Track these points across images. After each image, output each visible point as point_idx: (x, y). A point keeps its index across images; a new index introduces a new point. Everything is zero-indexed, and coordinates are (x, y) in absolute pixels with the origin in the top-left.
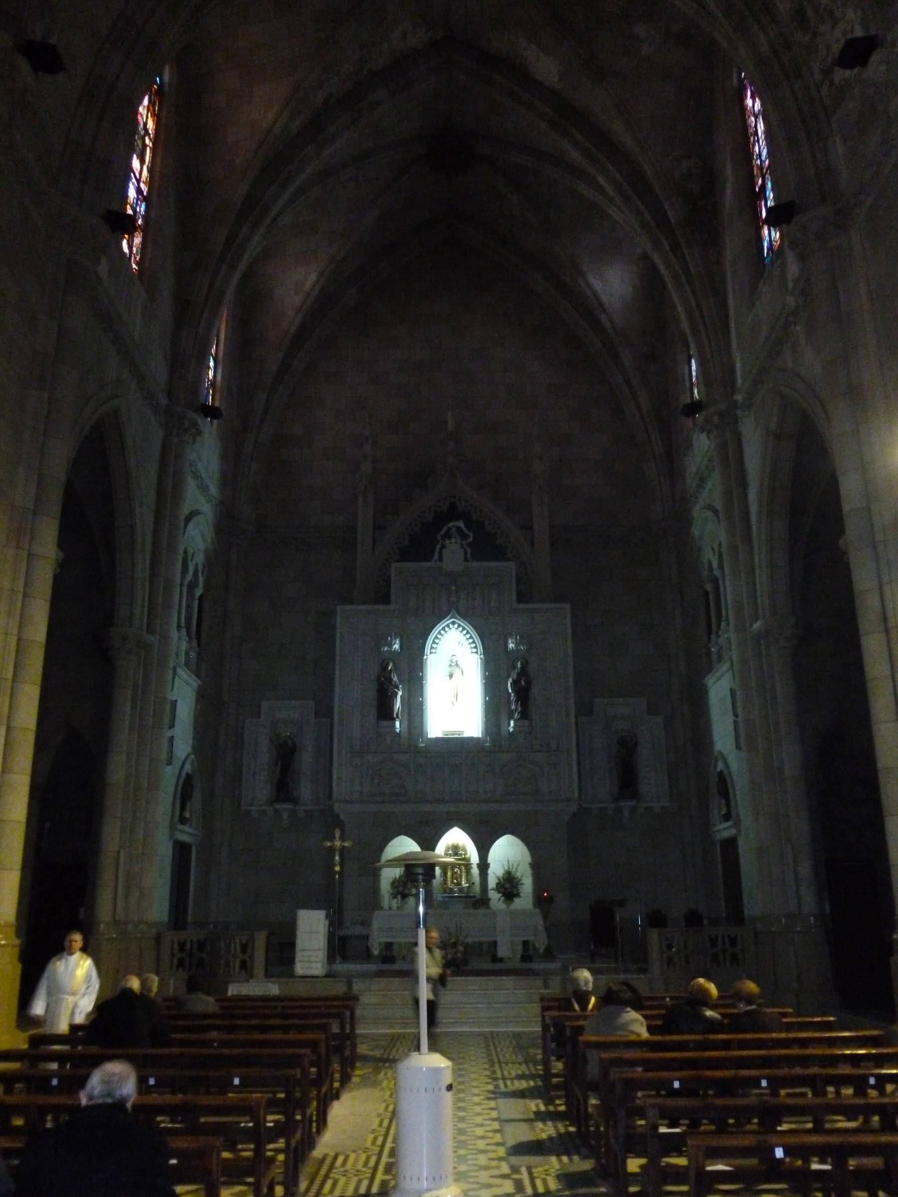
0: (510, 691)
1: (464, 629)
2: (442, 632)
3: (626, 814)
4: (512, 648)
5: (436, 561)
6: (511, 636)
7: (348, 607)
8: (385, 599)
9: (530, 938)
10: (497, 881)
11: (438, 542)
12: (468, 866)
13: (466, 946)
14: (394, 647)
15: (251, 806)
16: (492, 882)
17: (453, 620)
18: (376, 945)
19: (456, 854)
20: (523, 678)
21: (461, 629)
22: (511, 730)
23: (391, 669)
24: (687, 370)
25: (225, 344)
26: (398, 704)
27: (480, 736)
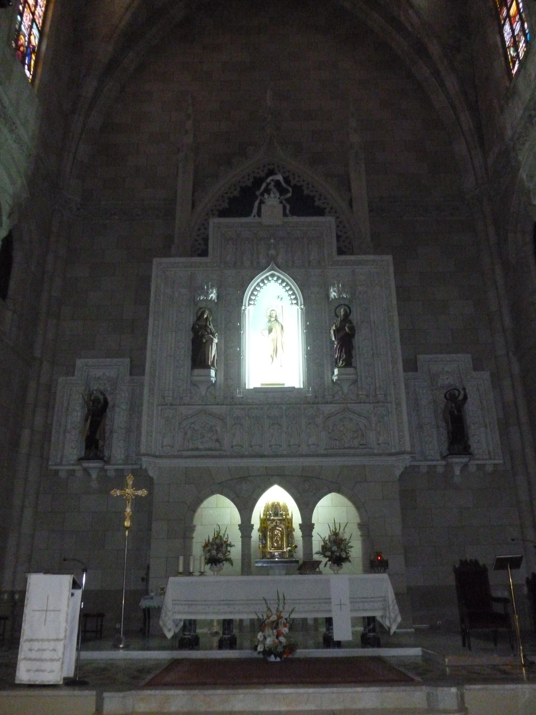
0: (333, 339)
1: (283, 281)
2: (261, 285)
3: (457, 472)
4: (335, 296)
5: (254, 216)
6: (334, 285)
7: (164, 260)
8: (204, 253)
9: (377, 614)
10: (323, 544)
11: (257, 197)
12: (289, 530)
13: (293, 625)
14: (210, 296)
15: (61, 464)
16: (317, 545)
17: (272, 272)
18: (170, 624)
19: (276, 514)
20: (347, 325)
21: (280, 281)
22: (335, 378)
23: (207, 317)
24: (498, 39)
25: (52, 21)
26: (213, 351)
27: (302, 387)
